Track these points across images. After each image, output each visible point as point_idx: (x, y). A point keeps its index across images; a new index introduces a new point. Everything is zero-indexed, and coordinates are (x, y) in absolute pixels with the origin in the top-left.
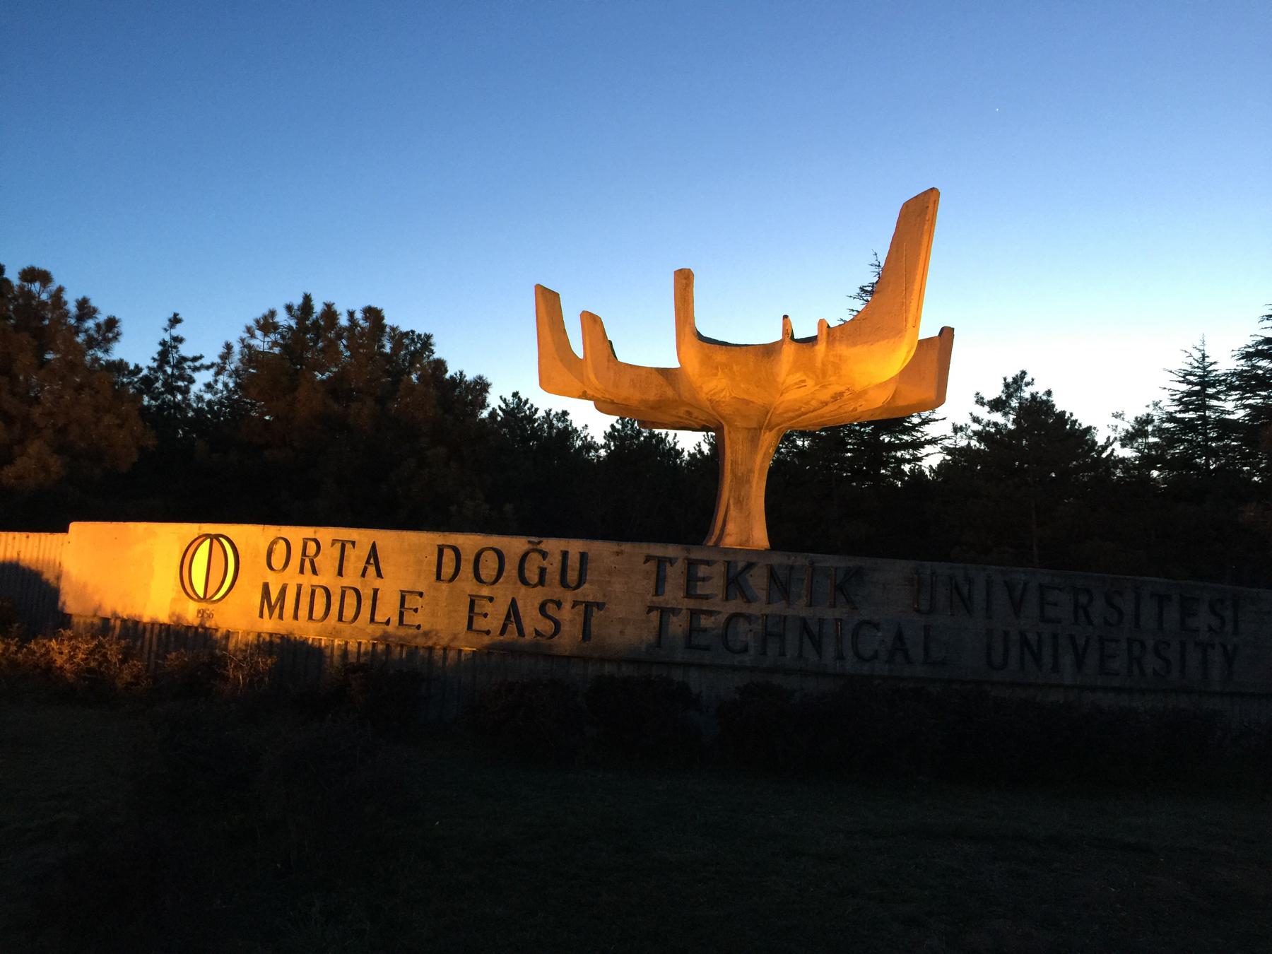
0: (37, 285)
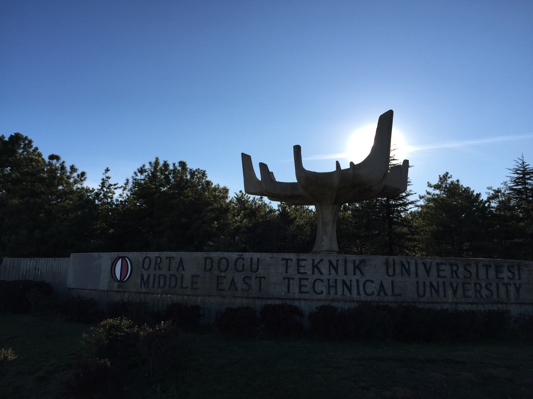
0: (55, 160)
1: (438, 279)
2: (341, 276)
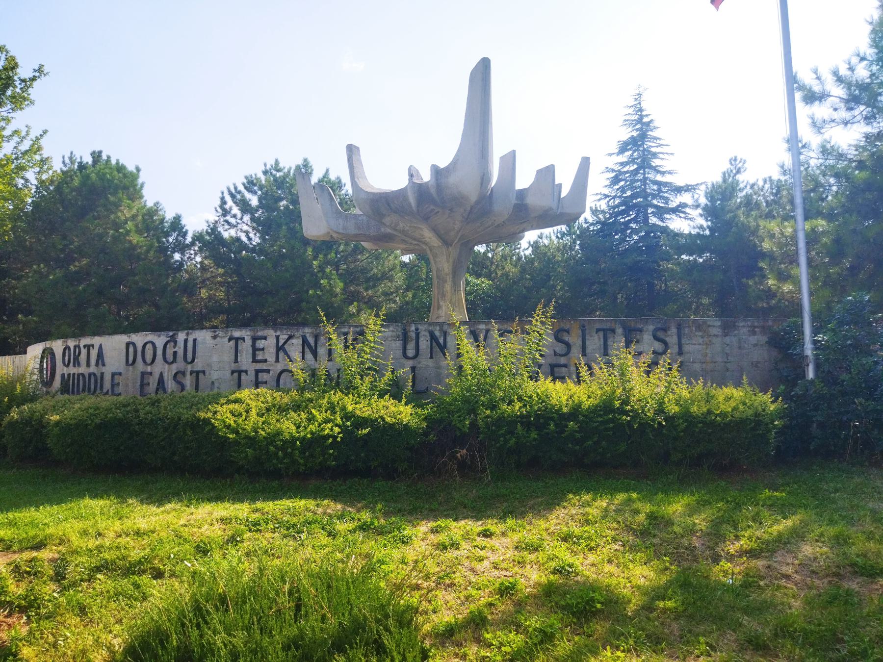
1: (253, 373)
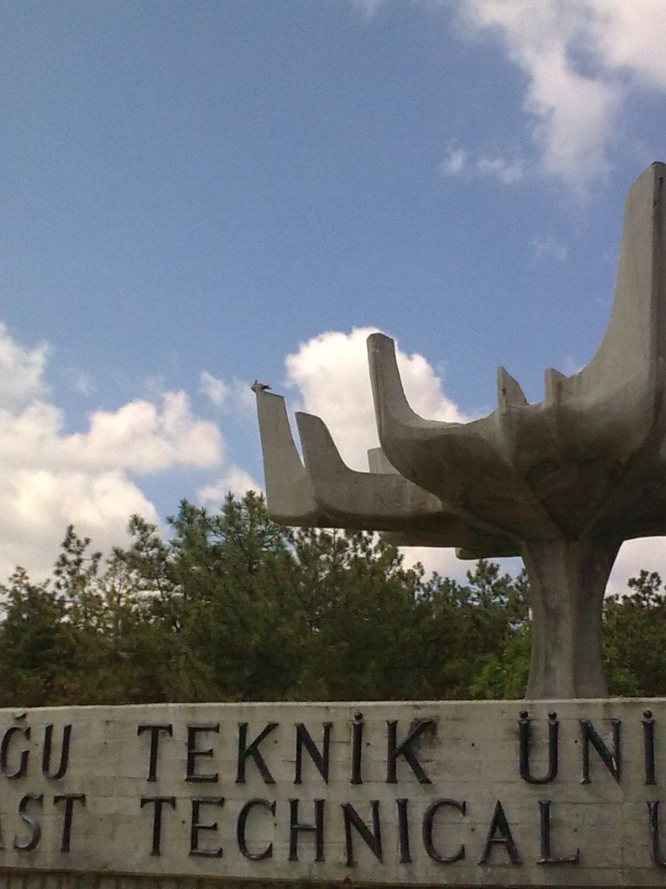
2: (340, 792)
